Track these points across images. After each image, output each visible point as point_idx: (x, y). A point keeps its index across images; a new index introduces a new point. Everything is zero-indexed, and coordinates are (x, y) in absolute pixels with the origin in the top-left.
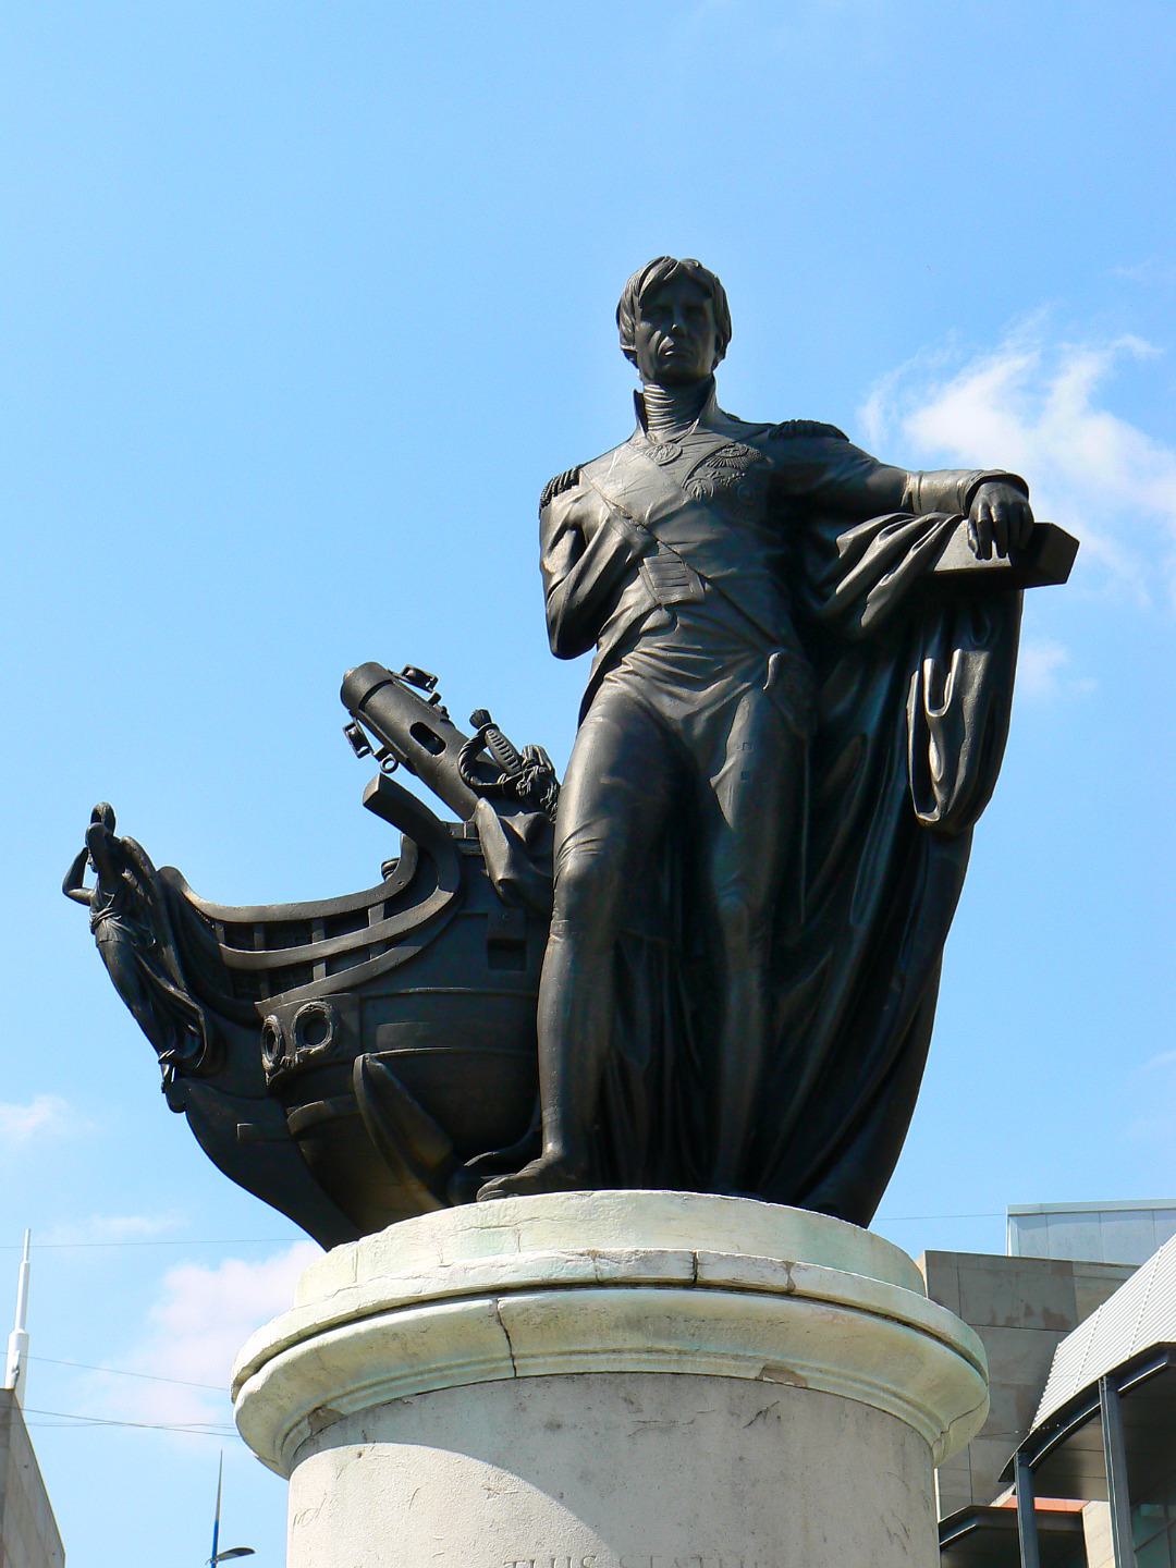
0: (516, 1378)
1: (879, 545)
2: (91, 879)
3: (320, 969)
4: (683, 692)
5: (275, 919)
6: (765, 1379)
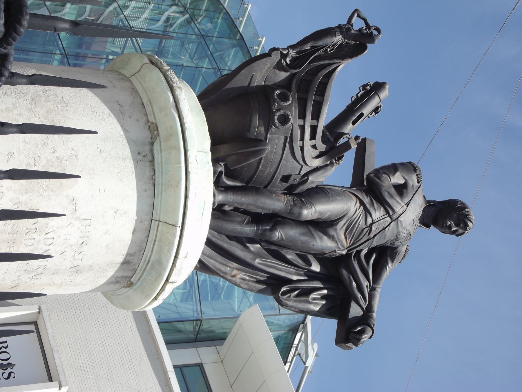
0: (152, 219)
3: (301, 122)
4: (344, 228)
5: (323, 107)
6: (129, 282)
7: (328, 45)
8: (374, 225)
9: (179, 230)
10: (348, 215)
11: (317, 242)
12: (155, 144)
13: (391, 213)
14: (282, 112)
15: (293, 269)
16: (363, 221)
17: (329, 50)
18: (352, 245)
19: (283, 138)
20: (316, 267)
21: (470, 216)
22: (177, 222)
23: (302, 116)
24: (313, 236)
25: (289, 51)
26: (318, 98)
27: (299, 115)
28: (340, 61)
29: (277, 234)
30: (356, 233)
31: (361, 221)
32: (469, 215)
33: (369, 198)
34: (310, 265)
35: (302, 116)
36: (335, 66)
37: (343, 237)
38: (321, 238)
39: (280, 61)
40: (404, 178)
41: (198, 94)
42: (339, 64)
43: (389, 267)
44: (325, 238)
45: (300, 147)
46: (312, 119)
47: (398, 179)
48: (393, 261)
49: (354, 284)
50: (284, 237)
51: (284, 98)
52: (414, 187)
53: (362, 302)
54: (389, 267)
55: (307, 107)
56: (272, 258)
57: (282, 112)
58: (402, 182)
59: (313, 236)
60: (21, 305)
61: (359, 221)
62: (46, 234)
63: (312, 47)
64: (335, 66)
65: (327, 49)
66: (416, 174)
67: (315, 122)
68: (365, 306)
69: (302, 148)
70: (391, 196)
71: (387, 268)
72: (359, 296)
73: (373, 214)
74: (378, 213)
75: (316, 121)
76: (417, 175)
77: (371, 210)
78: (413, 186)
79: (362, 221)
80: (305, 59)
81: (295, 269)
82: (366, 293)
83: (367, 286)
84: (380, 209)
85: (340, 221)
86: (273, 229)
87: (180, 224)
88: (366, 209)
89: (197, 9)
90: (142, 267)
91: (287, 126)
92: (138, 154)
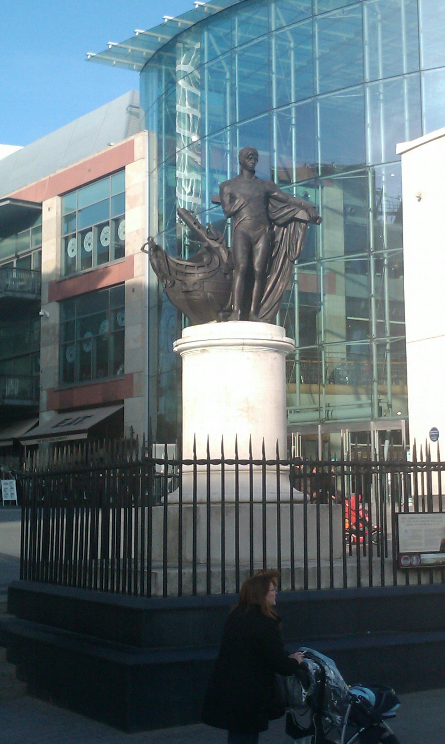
1: (286, 211)
2: (147, 248)
46: (194, 269)
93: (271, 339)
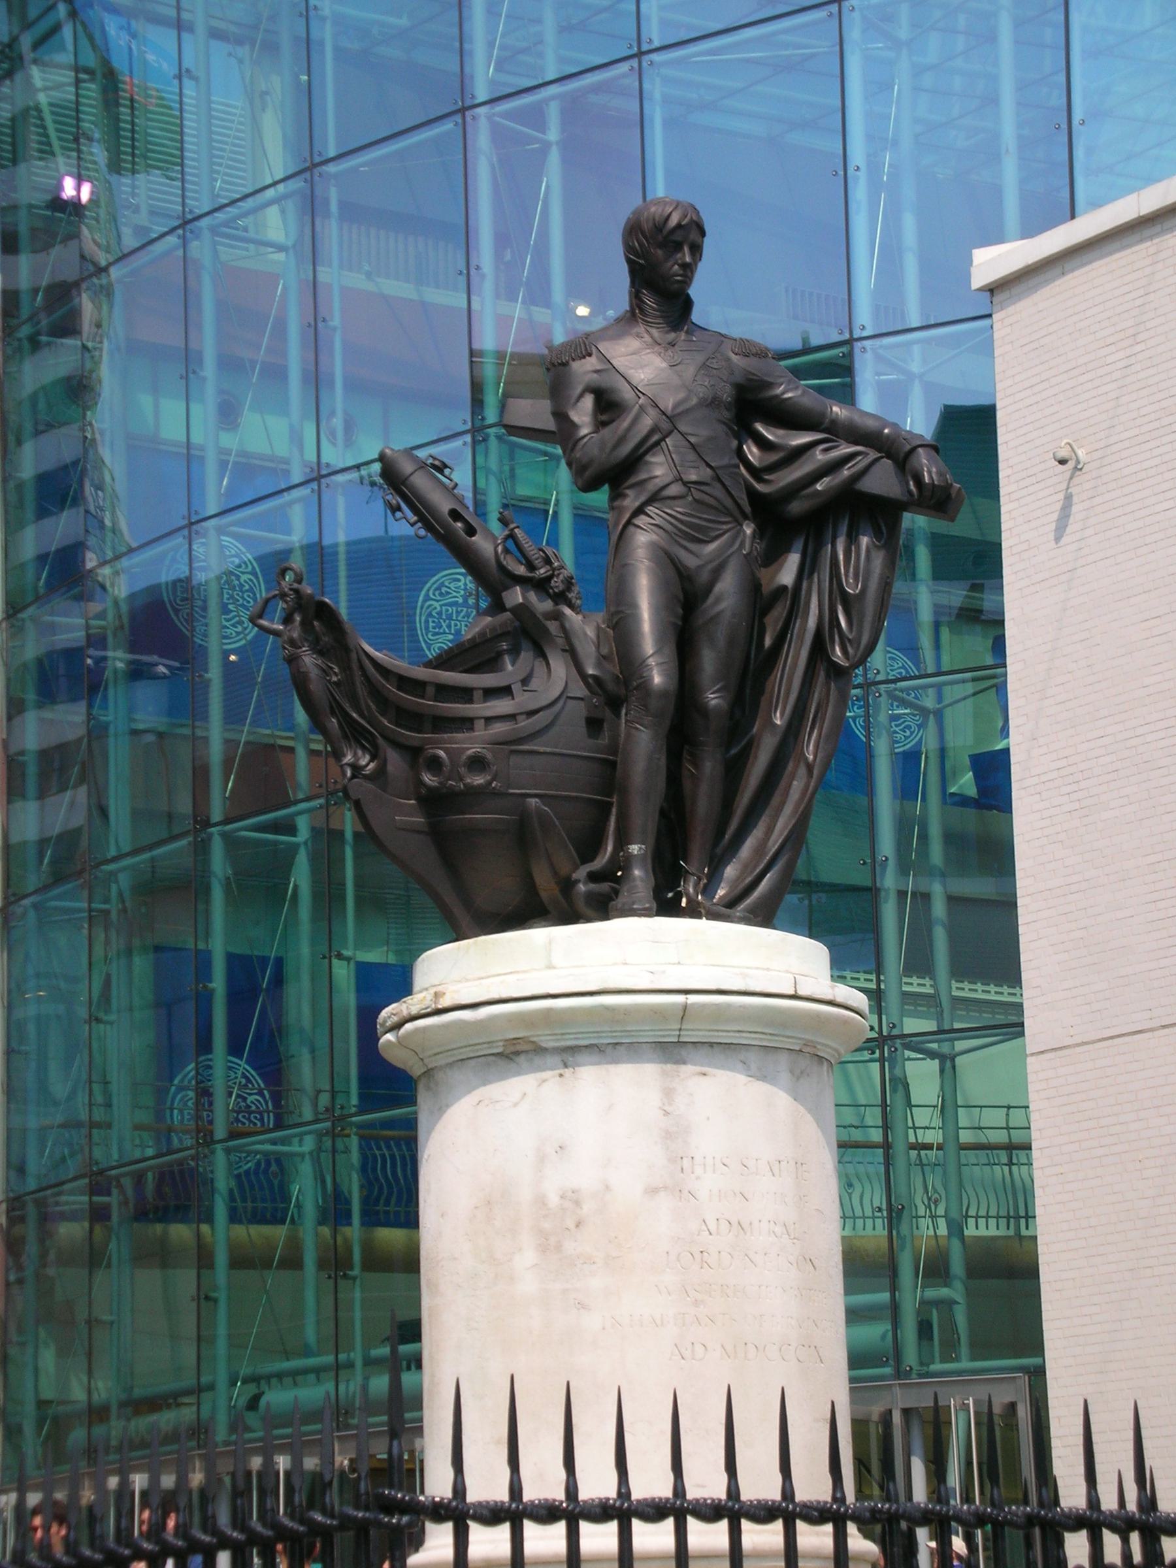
1: (820, 456)
3: (479, 724)
7: (328, 689)
8: (686, 478)
9: (693, 999)
10: (666, 547)
11: (722, 611)
12: (544, 1045)
13: (655, 438)
14: (463, 770)
15: (794, 624)
16: (678, 507)
17: (335, 679)
18: (731, 515)
19: (514, 759)
20: (787, 574)
21: (657, 219)
22: (674, 1005)
23: (467, 723)
24: (715, 618)
25: (346, 764)
26: (430, 691)
27: (466, 703)
28: (354, 656)
29: (713, 702)
30: (705, 516)
31: (678, 509)
32: (654, 220)
33: (628, 492)
34: (785, 588)
35: (467, 723)
36: (367, 662)
37: (712, 546)
38: (718, 600)
39: (367, 777)
40: (581, 396)
41: (454, 560)
42: (361, 652)
43: (783, 393)
44: (719, 587)
45: (527, 718)
47: (583, 414)
48: (770, 385)
49: (819, 487)
50: (718, 686)
51: (435, 764)
52: (599, 368)
53: (860, 463)
54: (783, 393)
55: (450, 715)
56: (772, 677)
57: (463, 770)
58: (588, 402)
59: (715, 618)
60: (829, 1407)
61: (679, 516)
62: (711, 1234)
63: (333, 713)
64: (367, 662)
65: (335, 683)
66: (571, 362)
67: (478, 695)
68: (868, 454)
69: (531, 713)
70: (622, 440)
71: (786, 396)
72: (846, 472)
73: (659, 483)
74: (659, 469)
75: (475, 693)
76: (574, 360)
77: (651, 487)
78: (597, 371)
79: (679, 509)
80: (379, 1091)
81: (796, 619)
82: (846, 449)
83: (826, 450)
84: (651, 463)
85: (680, 561)
86: (703, 711)
87: (680, 999)
88: (651, 500)
89: (181, 113)
90: (769, 1040)
91: (489, 756)
92: (562, 1079)
93: (792, 992)
